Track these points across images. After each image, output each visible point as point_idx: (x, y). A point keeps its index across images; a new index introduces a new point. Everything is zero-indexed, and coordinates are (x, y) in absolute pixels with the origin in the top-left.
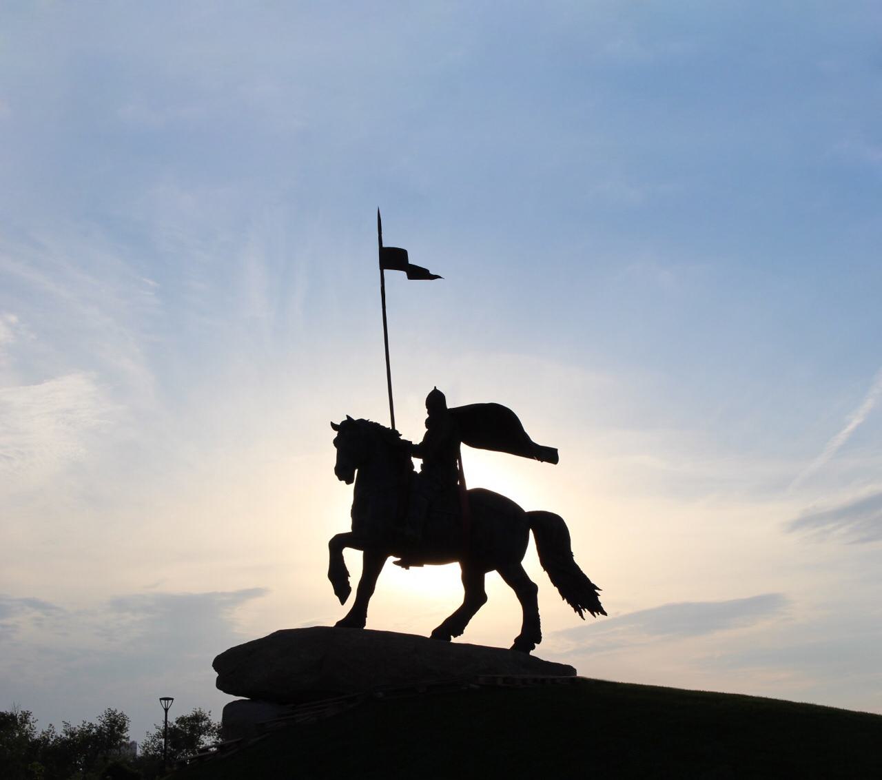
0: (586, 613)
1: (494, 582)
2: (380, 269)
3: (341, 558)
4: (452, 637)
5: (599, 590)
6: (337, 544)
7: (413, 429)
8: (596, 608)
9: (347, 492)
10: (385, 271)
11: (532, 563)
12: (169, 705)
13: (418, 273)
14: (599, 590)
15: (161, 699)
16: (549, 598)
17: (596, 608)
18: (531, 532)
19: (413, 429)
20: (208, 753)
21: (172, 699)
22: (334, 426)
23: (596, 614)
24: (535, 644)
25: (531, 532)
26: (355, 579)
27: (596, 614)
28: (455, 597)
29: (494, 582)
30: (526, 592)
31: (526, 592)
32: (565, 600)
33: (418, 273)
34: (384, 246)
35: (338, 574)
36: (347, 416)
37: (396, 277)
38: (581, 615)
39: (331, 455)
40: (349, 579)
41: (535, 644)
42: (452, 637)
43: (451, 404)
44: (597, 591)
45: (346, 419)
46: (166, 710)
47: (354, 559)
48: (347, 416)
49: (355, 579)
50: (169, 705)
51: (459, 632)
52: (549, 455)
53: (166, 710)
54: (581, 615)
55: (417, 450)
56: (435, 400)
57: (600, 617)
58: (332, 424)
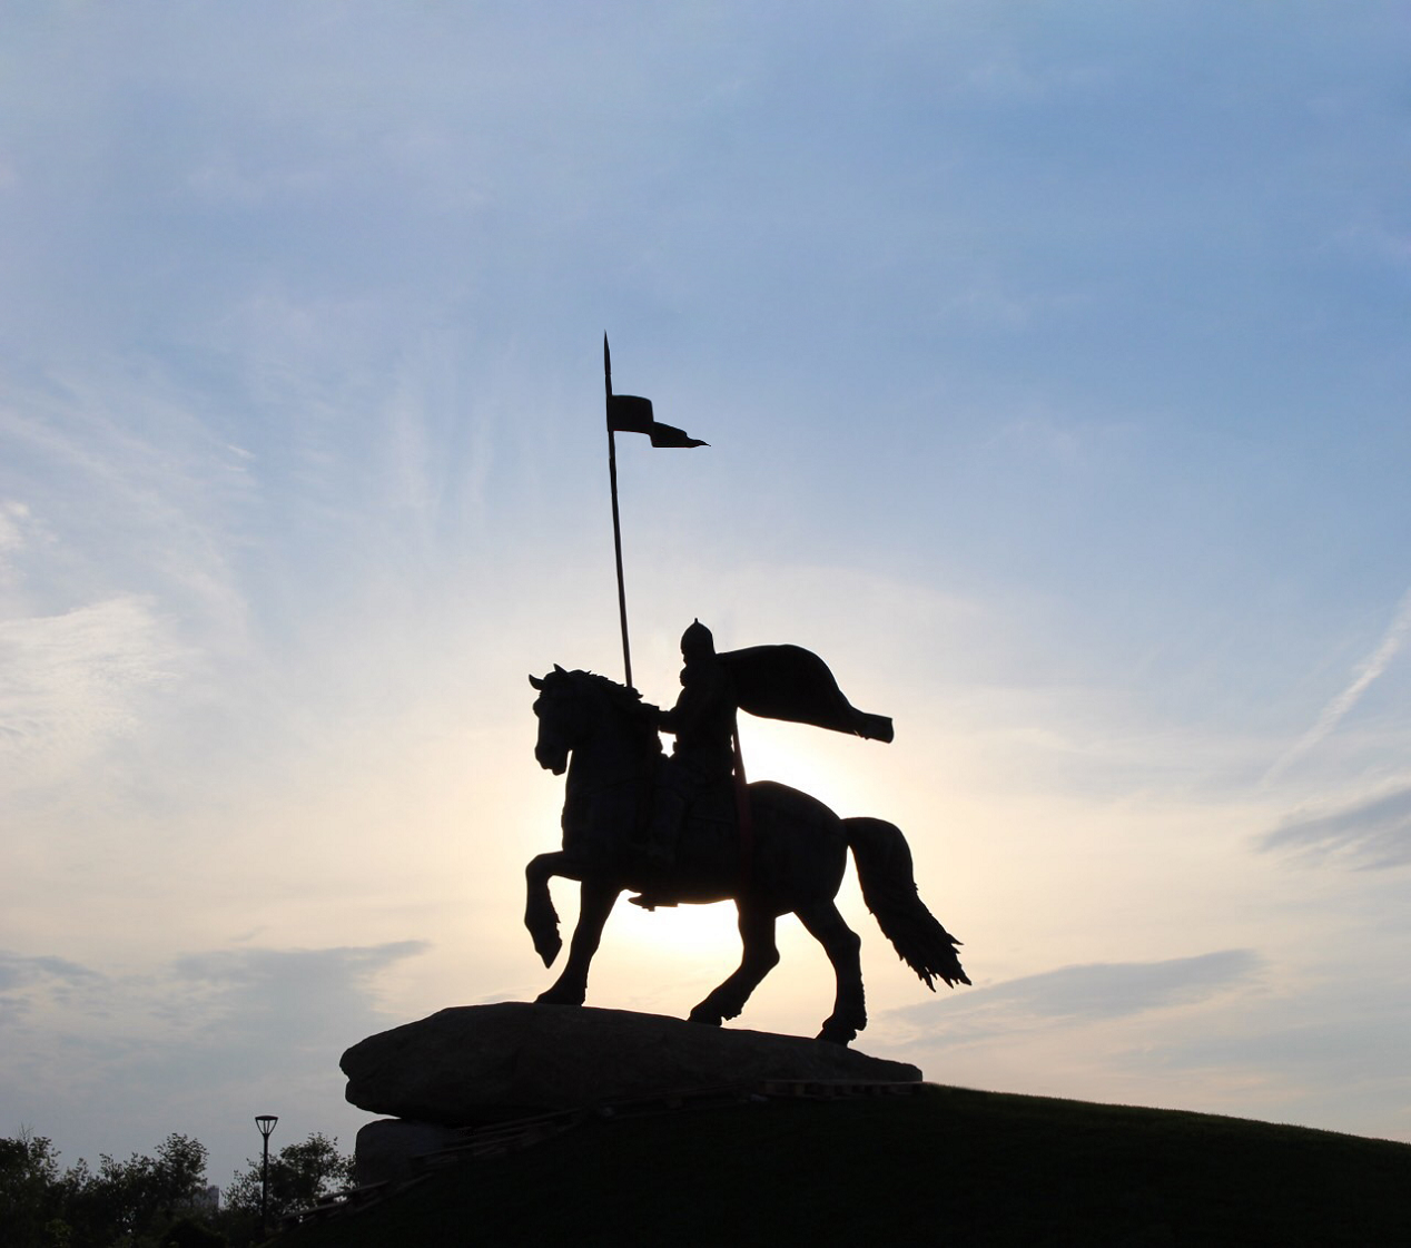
0: (938, 981)
1: (790, 930)
5: (958, 943)
6: (540, 871)
7: (661, 686)
8: (954, 973)
10: (616, 433)
11: (850, 901)
13: (668, 437)
14: (958, 943)
15: (257, 1119)
16: (879, 956)
17: (954, 973)
19: (661, 686)
21: (276, 1119)
22: (534, 682)
23: (953, 982)
26: (567, 927)
27: (953, 982)
28: (729, 954)
29: (790, 930)
30: (842, 947)
31: (842, 947)
32: (904, 960)
33: (668, 437)
35: (540, 918)
36: (556, 666)
37: (633, 443)
38: (929, 983)
44: (954, 945)
46: (266, 1136)
47: (566, 895)
48: (556, 666)
49: (567, 927)
52: (879, 729)
53: (266, 1136)
54: (929, 983)
56: (696, 641)
57: (960, 987)
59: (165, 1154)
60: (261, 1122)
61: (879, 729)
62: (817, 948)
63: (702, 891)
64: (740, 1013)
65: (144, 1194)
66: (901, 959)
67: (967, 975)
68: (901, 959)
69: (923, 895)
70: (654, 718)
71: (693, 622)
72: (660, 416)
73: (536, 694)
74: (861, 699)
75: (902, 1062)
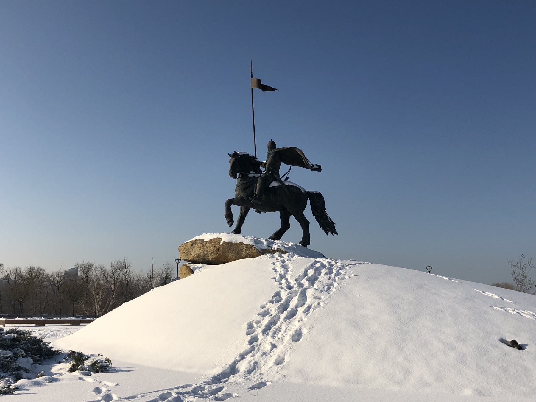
0: (330, 233)
1: (292, 219)
3: (280, 183)
6: (230, 203)
7: (263, 157)
8: (334, 232)
9: (235, 182)
11: (308, 212)
12: (179, 262)
14: (335, 224)
15: (175, 260)
16: (314, 226)
17: (334, 232)
18: (308, 199)
19: (263, 157)
20: (449, 278)
21: (432, 267)
22: (230, 155)
23: (333, 234)
24: (307, 245)
25: (308, 199)
26: (236, 217)
27: (333, 234)
28: (277, 225)
29: (292, 219)
30: (305, 224)
31: (305, 224)
32: (321, 228)
35: (229, 216)
36: (235, 151)
38: (327, 234)
39: (228, 167)
40: (233, 217)
41: (307, 245)
43: (279, 146)
45: (234, 152)
46: (178, 264)
47: (236, 210)
48: (235, 151)
49: (236, 217)
50: (179, 262)
52: (319, 169)
53: (178, 264)
55: (264, 165)
56: (273, 145)
58: (229, 154)
59: (455, 341)
60: (176, 260)
62: (298, 224)
63: (272, 209)
67: (337, 232)
69: (327, 211)
70: (260, 163)
73: (234, 152)
74: (312, 161)
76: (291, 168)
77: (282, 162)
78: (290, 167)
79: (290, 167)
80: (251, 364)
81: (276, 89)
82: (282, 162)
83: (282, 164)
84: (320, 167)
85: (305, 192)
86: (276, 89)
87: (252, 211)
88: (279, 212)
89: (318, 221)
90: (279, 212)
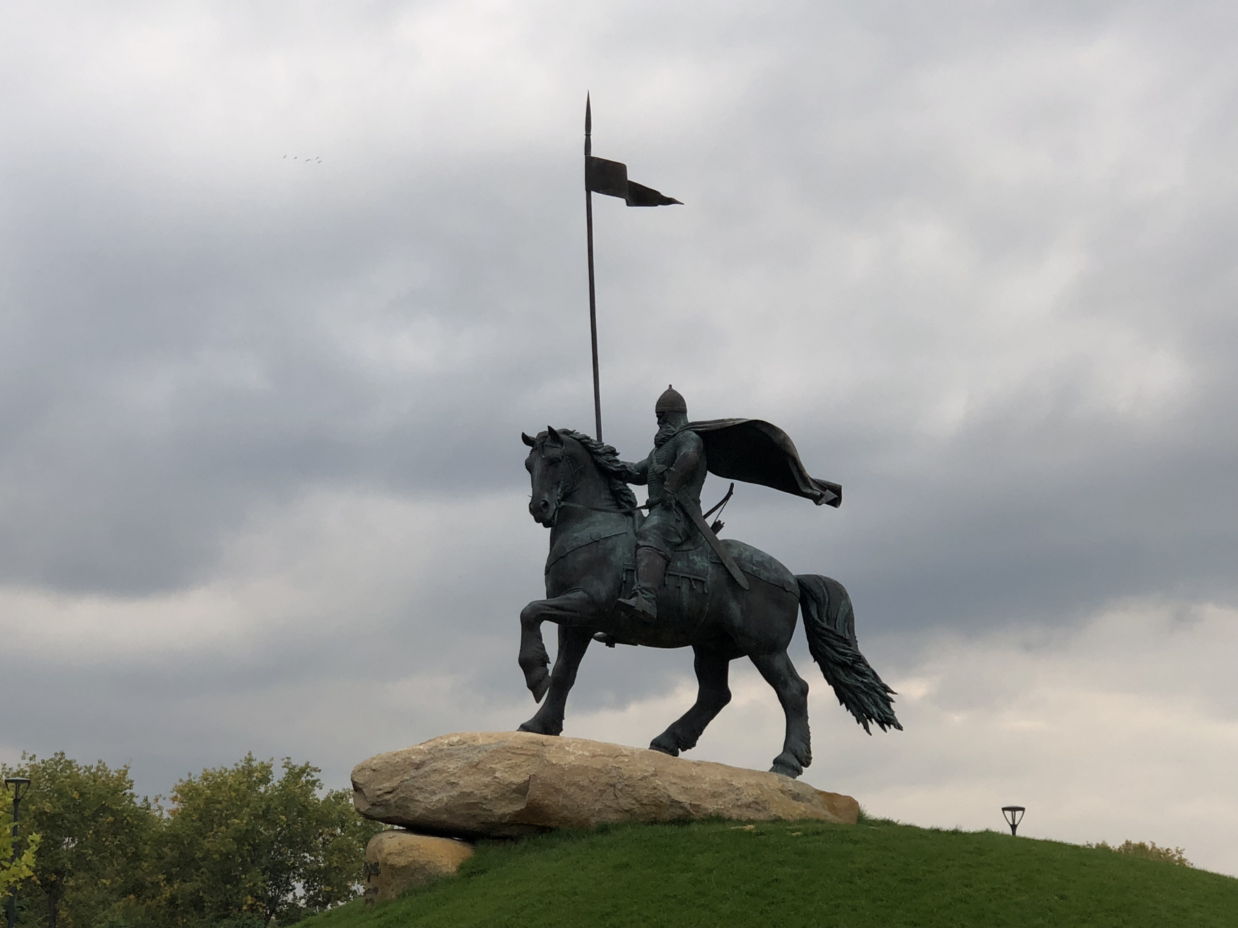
0: (874, 726)
2: (586, 190)
4: (679, 750)
5: (893, 692)
8: (887, 720)
10: (593, 194)
13: (643, 197)
14: (893, 692)
15: (1004, 809)
16: (820, 693)
17: (887, 720)
21: (1023, 809)
22: (526, 440)
23: (886, 726)
27: (886, 726)
28: (687, 696)
32: (844, 705)
33: (643, 197)
34: (595, 153)
35: (531, 661)
36: (549, 427)
37: (609, 206)
38: (866, 728)
42: (679, 750)
43: (693, 415)
44: (889, 695)
47: (550, 633)
48: (549, 427)
51: (689, 743)
52: (871, 734)
54: (866, 728)
57: (892, 730)
61: (871, 734)
64: (694, 745)
65: (299, 888)
66: (841, 704)
68: (841, 704)
71: (668, 388)
72: (632, 176)
75: (925, 823)
76: (733, 491)
77: (708, 472)
78: (732, 485)
79: (732, 485)
80: (211, 914)
81: (670, 201)
82: (708, 472)
83: (710, 476)
84: (837, 490)
85: (1154, 847)
86: (670, 201)
87: (595, 648)
88: (690, 647)
89: (1045, 842)
90: (690, 647)
